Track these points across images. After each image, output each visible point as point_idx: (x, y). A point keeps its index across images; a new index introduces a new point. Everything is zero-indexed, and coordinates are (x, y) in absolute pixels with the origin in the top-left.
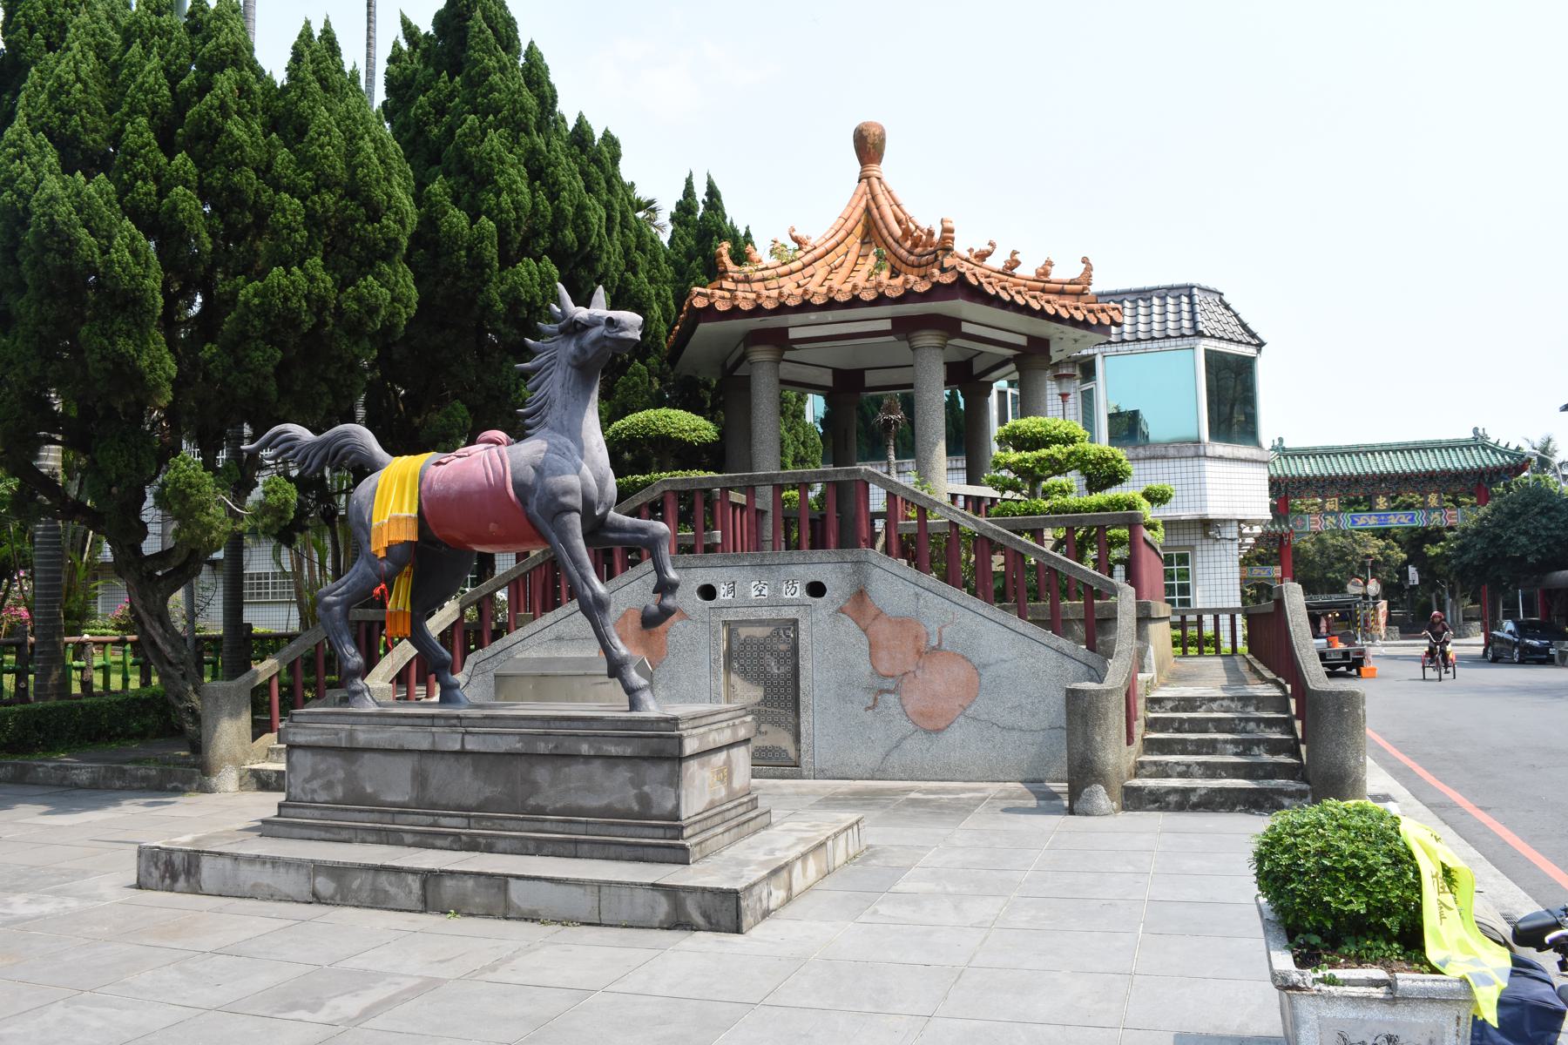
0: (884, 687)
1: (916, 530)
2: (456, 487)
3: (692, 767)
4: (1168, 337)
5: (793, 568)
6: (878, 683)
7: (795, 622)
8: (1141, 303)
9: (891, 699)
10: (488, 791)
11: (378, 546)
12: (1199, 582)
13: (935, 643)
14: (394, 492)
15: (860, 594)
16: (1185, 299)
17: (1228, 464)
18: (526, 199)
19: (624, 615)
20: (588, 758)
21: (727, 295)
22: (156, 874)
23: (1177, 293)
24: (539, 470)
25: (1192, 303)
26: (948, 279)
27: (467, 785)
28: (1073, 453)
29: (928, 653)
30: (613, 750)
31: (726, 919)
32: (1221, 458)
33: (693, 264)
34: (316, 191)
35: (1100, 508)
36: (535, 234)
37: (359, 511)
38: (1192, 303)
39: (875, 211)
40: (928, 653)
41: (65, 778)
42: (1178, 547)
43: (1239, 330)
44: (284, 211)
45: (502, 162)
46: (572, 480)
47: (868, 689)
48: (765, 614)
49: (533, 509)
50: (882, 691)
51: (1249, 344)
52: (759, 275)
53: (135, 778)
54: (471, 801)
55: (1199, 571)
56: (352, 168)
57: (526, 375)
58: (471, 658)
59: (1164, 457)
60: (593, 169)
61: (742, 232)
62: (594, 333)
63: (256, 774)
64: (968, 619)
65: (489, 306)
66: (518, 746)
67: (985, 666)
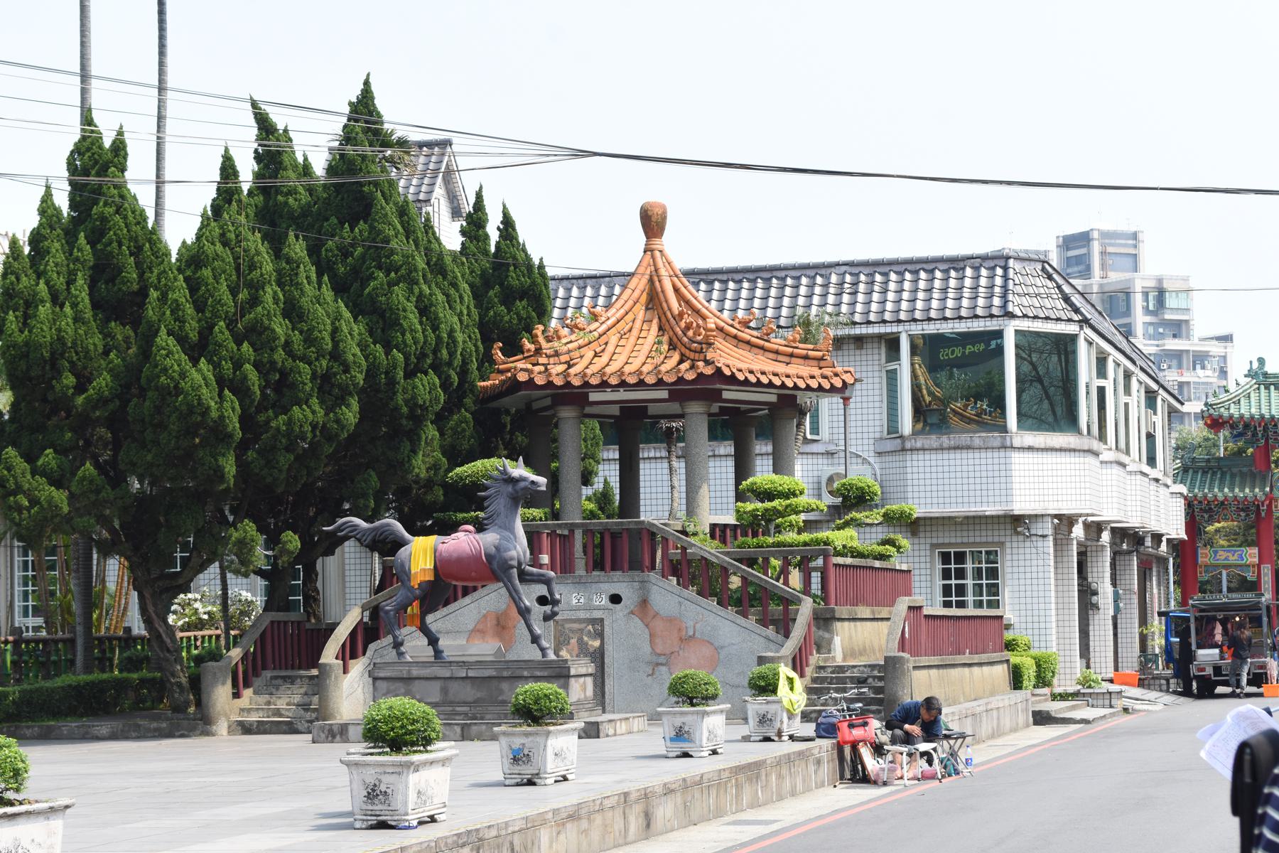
0: (659, 661)
1: (679, 557)
2: (455, 555)
3: (572, 681)
4: (976, 316)
5: (601, 585)
6: (655, 659)
7: (602, 620)
8: (953, 274)
9: (664, 669)
10: (479, 695)
11: (415, 583)
12: (1008, 582)
13: (691, 633)
14: (421, 554)
15: (644, 603)
16: (999, 271)
17: (1035, 454)
18: (420, 336)
19: (485, 616)
20: (526, 678)
21: (542, 368)
22: (323, 736)
23: (991, 264)
24: (497, 548)
25: (1005, 277)
26: (709, 371)
27: (469, 692)
28: (790, 505)
29: (686, 640)
30: (538, 674)
31: (593, 734)
32: (1030, 449)
33: (491, 293)
34: (317, 359)
35: (805, 544)
36: (424, 355)
37: (402, 565)
38: (1005, 277)
39: (657, 283)
40: (686, 640)
41: (87, 733)
42: (986, 544)
43: (1060, 304)
44: (300, 373)
45: (405, 310)
46: (513, 553)
47: (649, 663)
48: (582, 615)
49: (495, 566)
50: (658, 664)
51: (1070, 320)
52: (565, 349)
53: (149, 730)
54: (470, 699)
55: (1008, 570)
56: (336, 343)
57: (486, 498)
58: (372, 647)
59: (968, 448)
60: (452, 291)
61: (537, 262)
62: (522, 484)
63: (241, 724)
64: (712, 619)
65: (397, 409)
66: (494, 674)
67: (722, 647)
